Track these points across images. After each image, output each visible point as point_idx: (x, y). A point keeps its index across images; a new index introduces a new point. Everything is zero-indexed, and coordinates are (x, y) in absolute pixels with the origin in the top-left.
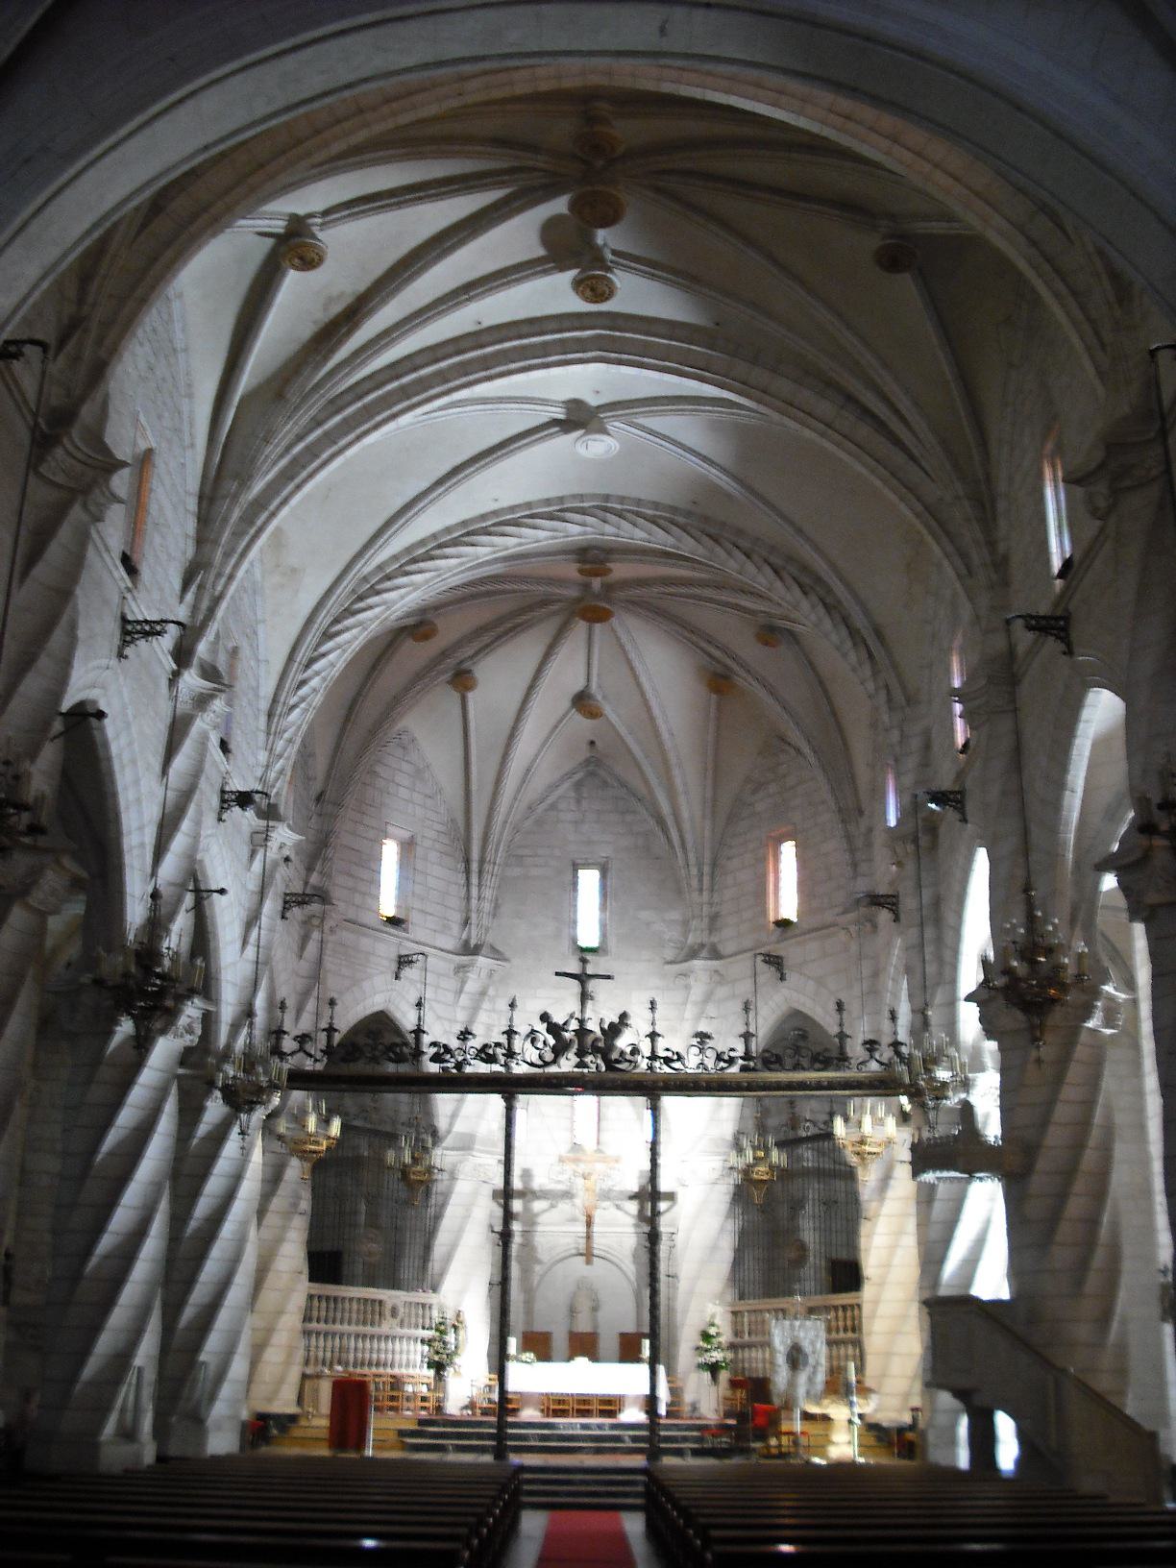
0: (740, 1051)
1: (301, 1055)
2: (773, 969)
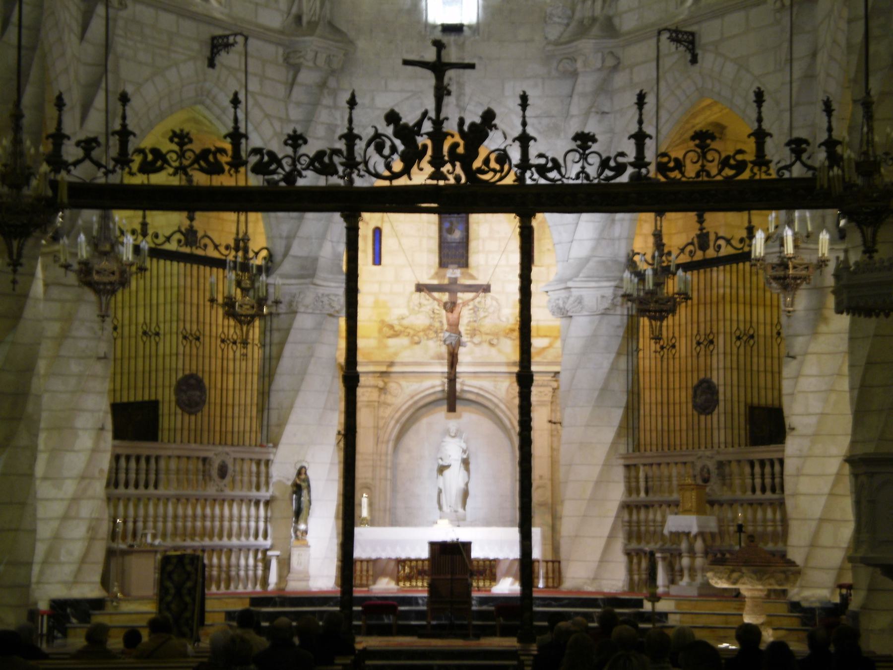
0: (631, 157)
1: (87, 164)
2: (682, 48)
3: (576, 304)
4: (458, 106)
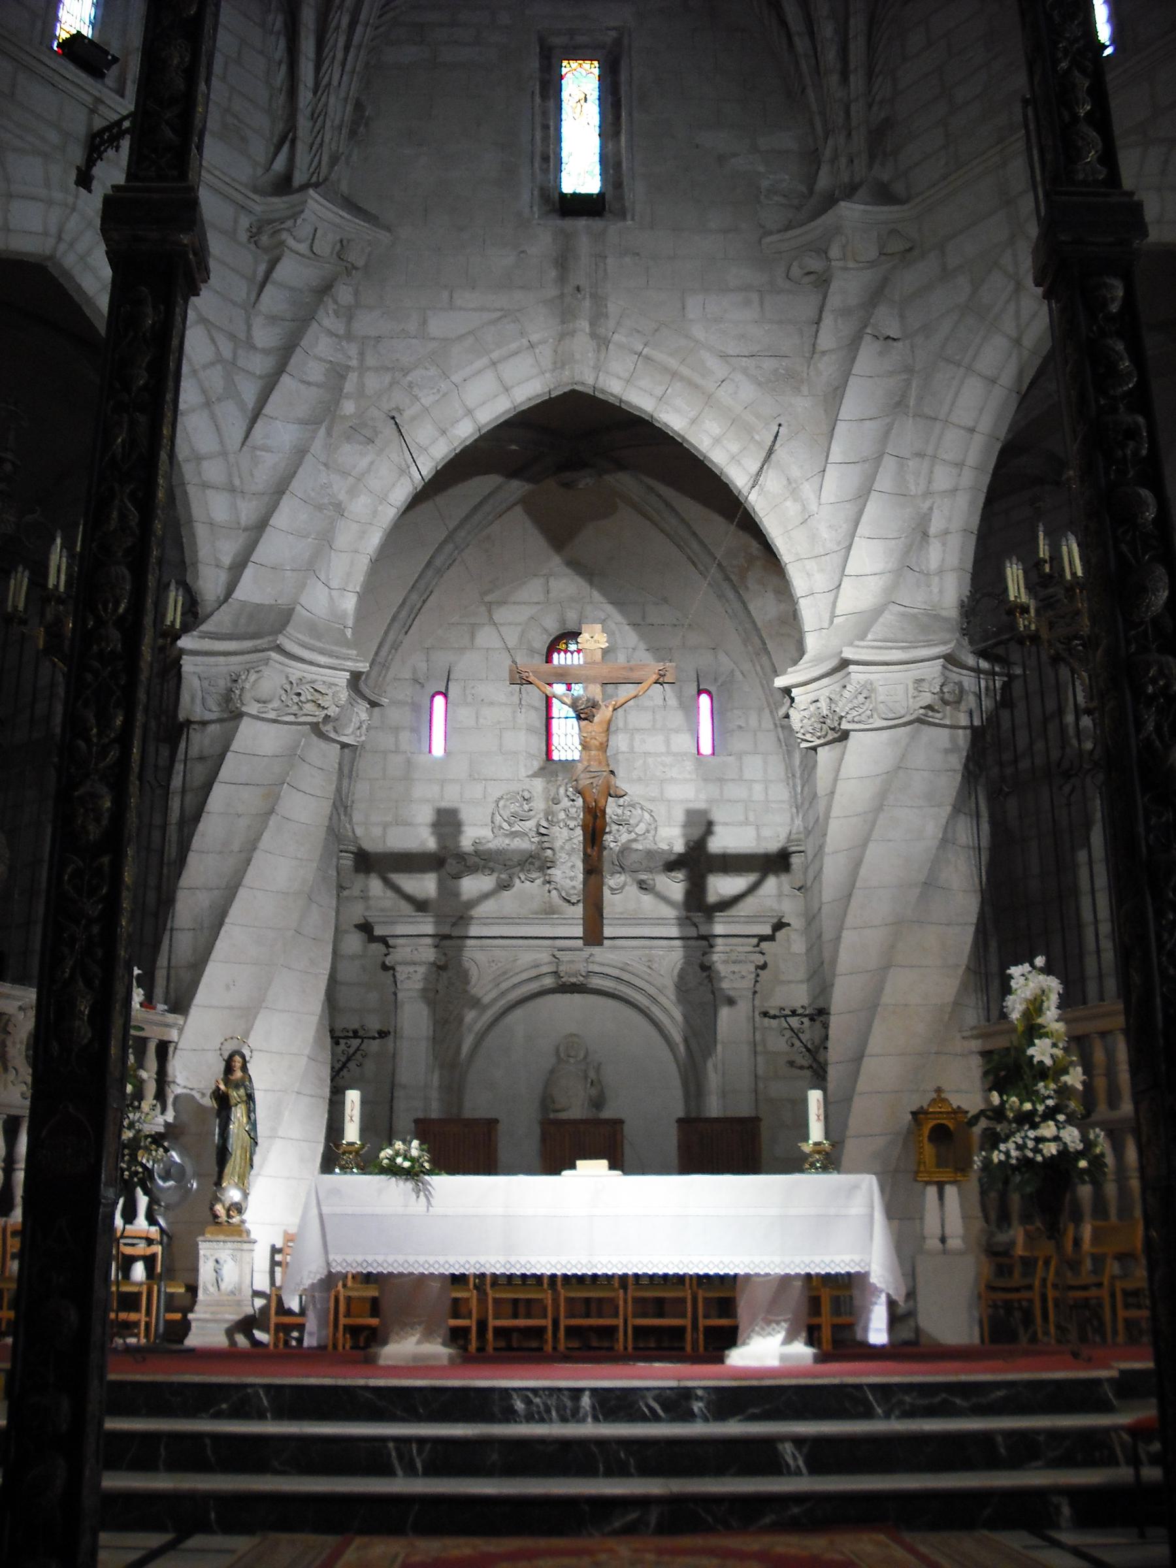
3: (861, 698)
4: (593, 335)
